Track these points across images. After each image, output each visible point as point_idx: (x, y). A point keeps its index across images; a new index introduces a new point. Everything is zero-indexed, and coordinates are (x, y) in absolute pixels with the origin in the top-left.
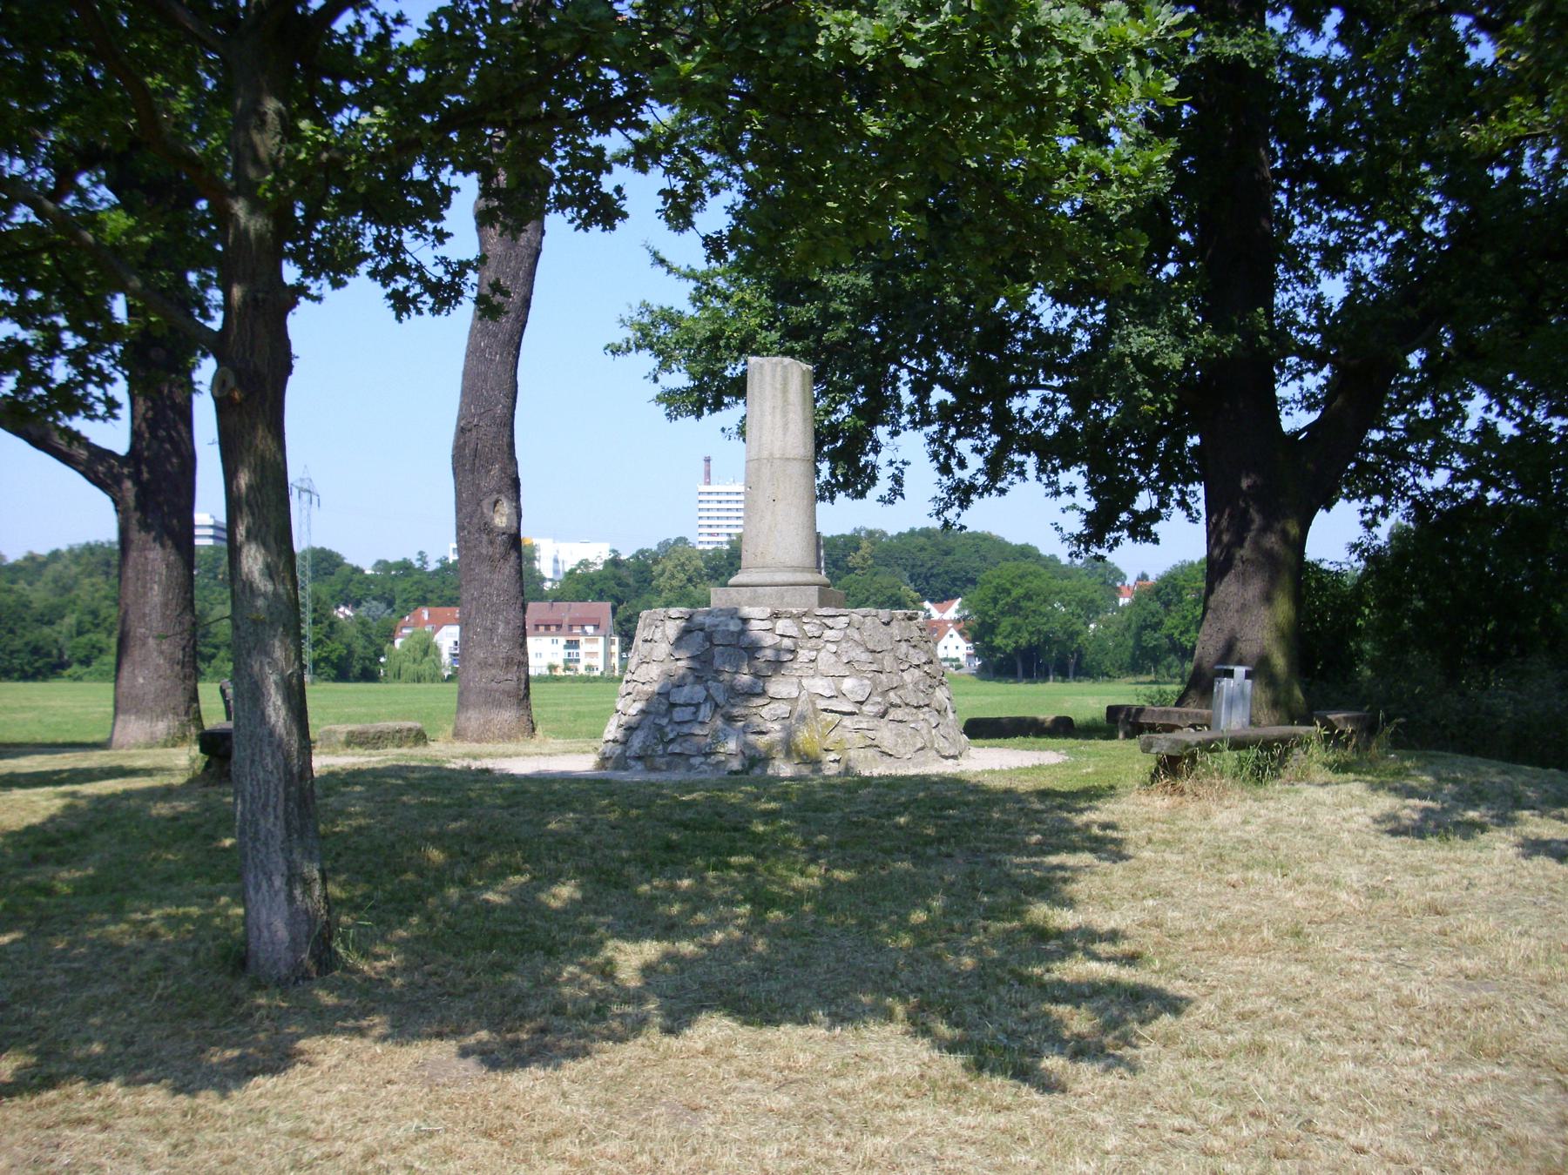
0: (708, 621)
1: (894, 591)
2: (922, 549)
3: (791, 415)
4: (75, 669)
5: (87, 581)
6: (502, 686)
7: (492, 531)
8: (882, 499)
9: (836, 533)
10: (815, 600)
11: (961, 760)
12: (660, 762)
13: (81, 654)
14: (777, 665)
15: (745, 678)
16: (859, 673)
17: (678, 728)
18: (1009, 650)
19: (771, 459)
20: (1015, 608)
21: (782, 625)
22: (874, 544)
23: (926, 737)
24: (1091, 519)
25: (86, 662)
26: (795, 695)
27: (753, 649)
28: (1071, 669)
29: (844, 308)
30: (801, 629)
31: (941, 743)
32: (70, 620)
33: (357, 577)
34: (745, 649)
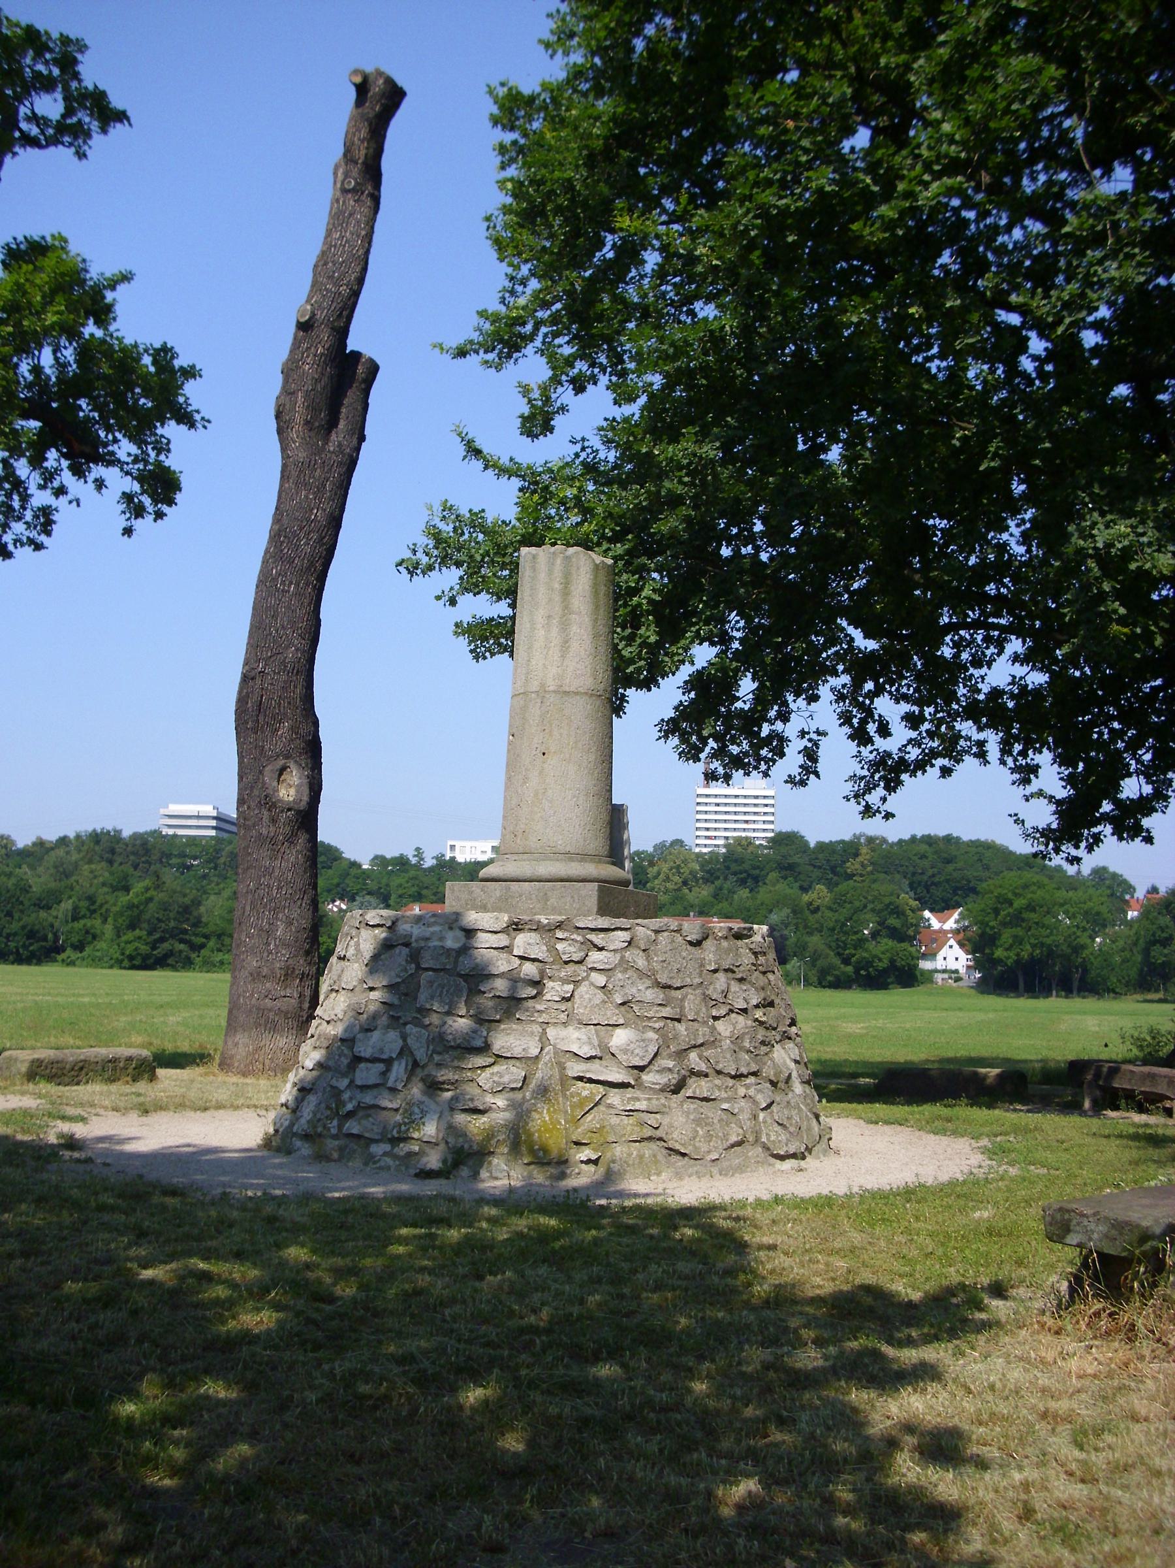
0: (416, 931)
1: (894, 898)
2: (923, 857)
3: (574, 629)
4: (69, 953)
5: (86, 867)
6: (278, 1003)
7: (274, 805)
8: (791, 780)
9: (835, 838)
10: (593, 902)
11: (810, 1162)
12: (331, 1144)
13: (75, 939)
14: (511, 1005)
15: (461, 1023)
16: (639, 1022)
17: (359, 1096)
18: (1009, 962)
19: (542, 692)
20: (1017, 919)
21: (524, 942)
22: (873, 850)
23: (748, 1125)
24: (1064, 809)
25: (79, 947)
26: (534, 1052)
27: (477, 977)
28: (1076, 984)
29: (680, 489)
30: (552, 949)
31: (774, 1136)
32: (67, 905)
33: (353, 871)
34: (466, 977)
